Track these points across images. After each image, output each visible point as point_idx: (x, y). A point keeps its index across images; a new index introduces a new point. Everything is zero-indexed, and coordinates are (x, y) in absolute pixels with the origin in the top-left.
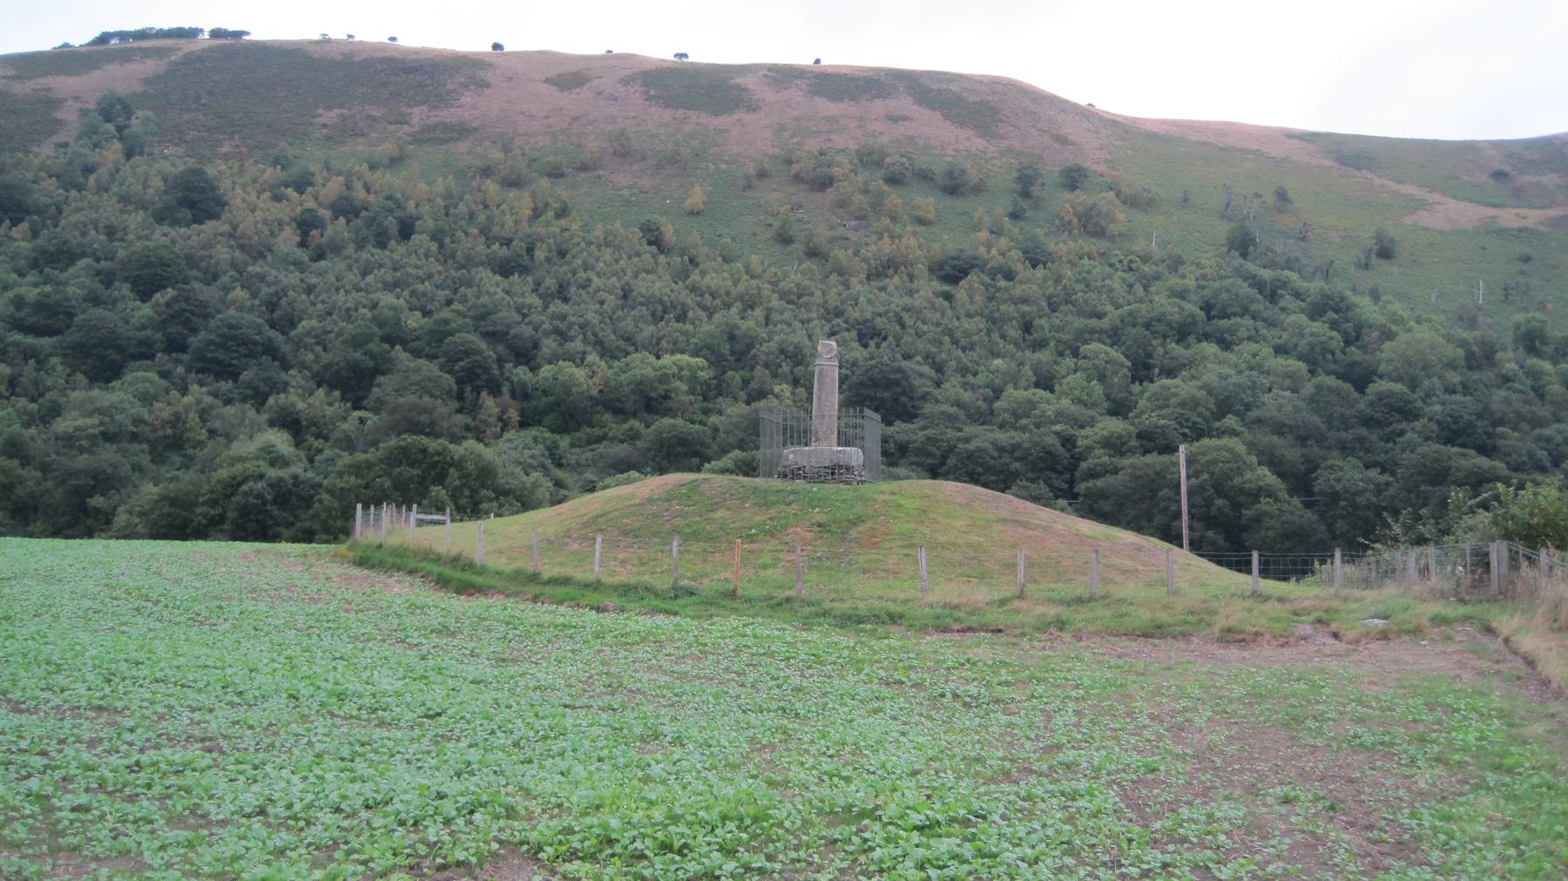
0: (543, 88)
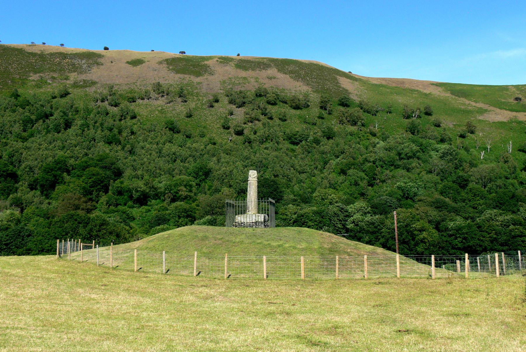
0: (125, 65)
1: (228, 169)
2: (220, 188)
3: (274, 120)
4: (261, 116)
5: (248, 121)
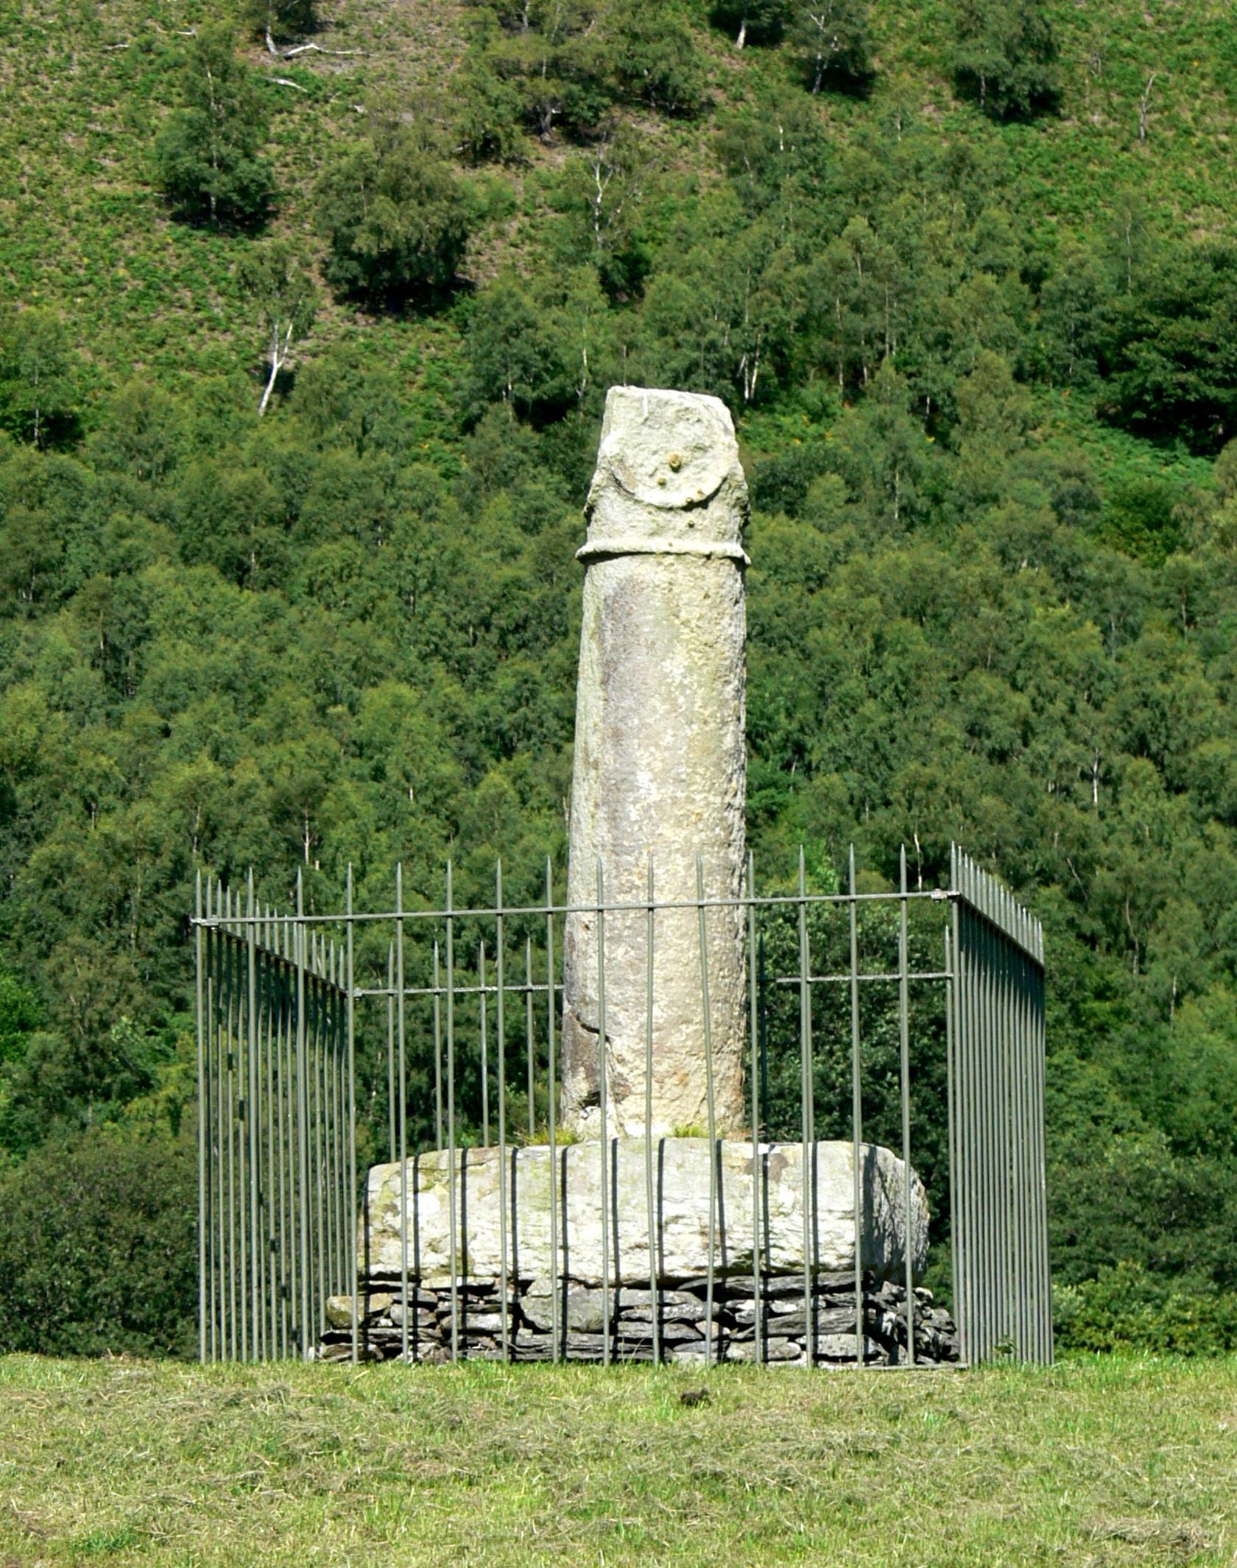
1: (246, 774)
2: (139, 1043)
3: (884, 103)
4: (707, 43)
5: (531, 121)
